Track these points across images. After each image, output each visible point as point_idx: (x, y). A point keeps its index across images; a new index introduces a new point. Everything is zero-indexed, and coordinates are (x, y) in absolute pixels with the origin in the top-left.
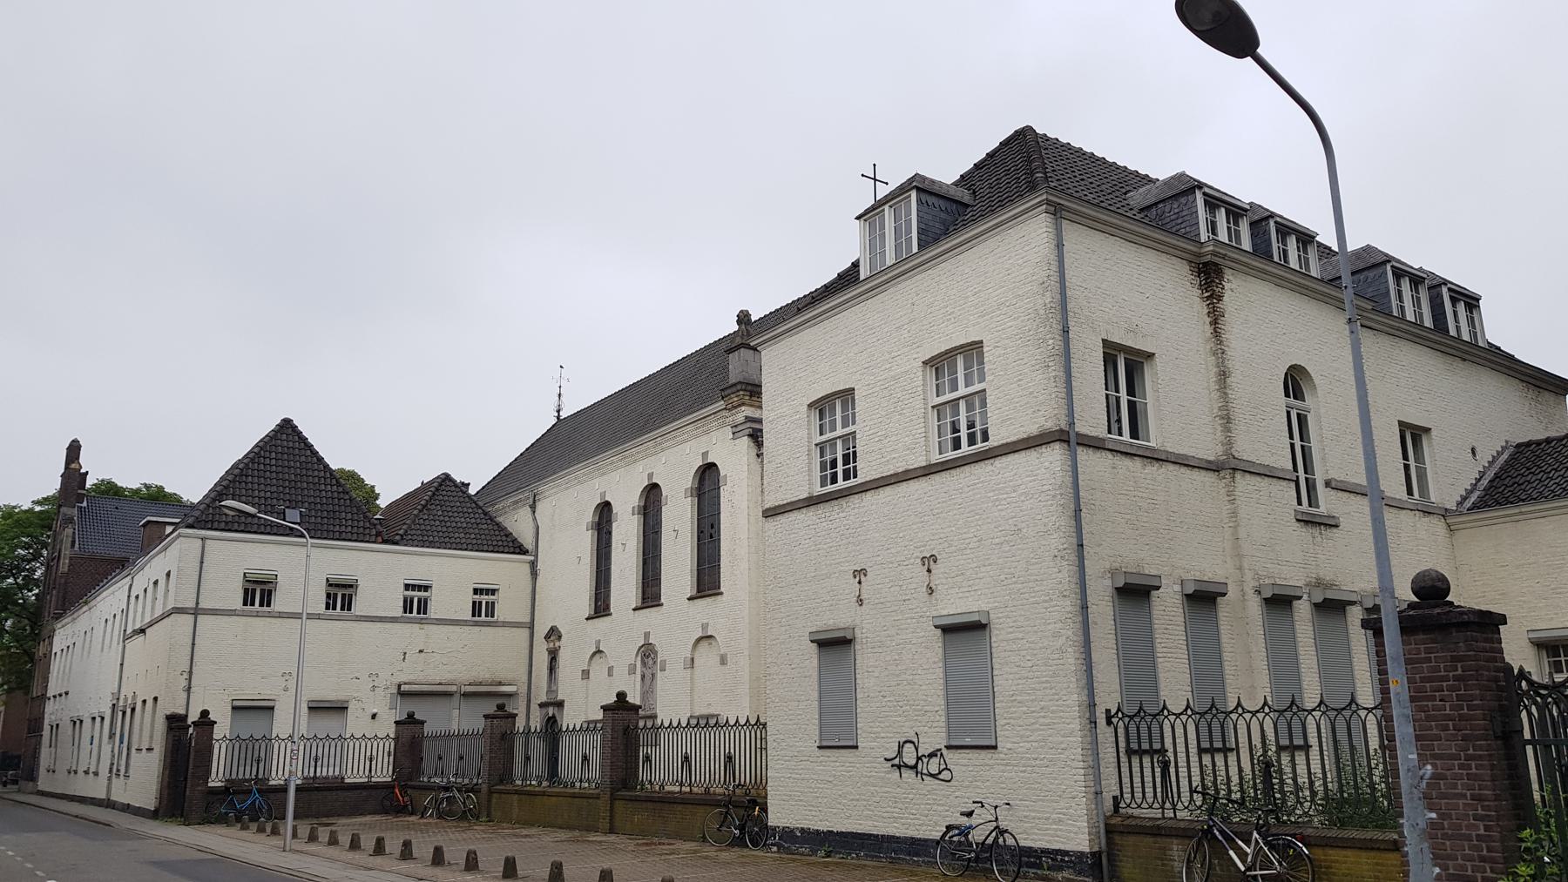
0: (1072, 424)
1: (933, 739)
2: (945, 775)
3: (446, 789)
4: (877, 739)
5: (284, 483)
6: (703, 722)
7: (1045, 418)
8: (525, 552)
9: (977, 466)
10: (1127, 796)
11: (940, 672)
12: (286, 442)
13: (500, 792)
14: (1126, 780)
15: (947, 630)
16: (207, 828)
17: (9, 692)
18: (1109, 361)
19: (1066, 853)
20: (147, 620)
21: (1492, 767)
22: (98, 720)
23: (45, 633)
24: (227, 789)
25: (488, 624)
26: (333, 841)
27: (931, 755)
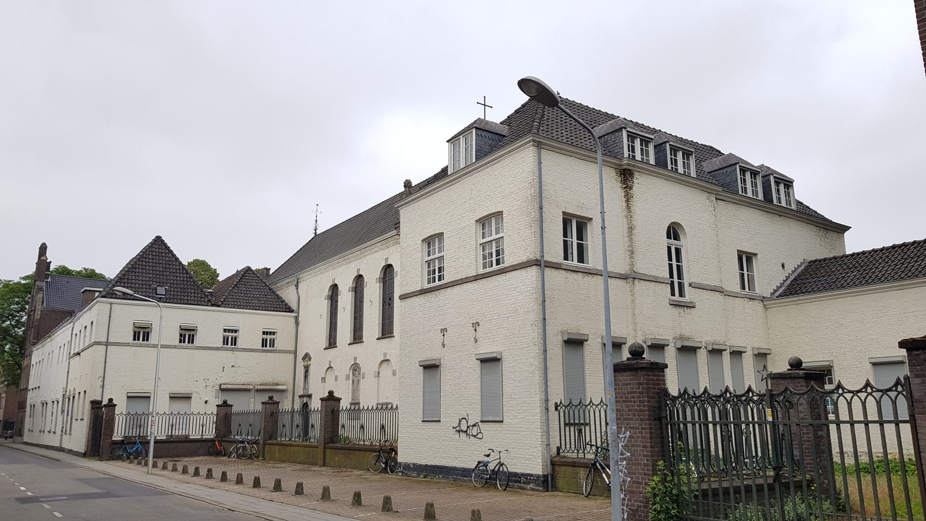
0: (542, 256)
1: (475, 418)
2: (480, 436)
3: (242, 442)
4: (449, 419)
6: (384, 407)
7: (530, 253)
8: (292, 311)
10: (563, 447)
11: (479, 383)
12: (158, 252)
13: (270, 444)
14: (563, 438)
15: (483, 361)
16: (111, 462)
17: (8, 386)
18: (566, 222)
19: (531, 475)
21: (651, 433)
23: (27, 353)
24: (123, 441)
25: (271, 351)
26: (175, 469)
27: (474, 426)
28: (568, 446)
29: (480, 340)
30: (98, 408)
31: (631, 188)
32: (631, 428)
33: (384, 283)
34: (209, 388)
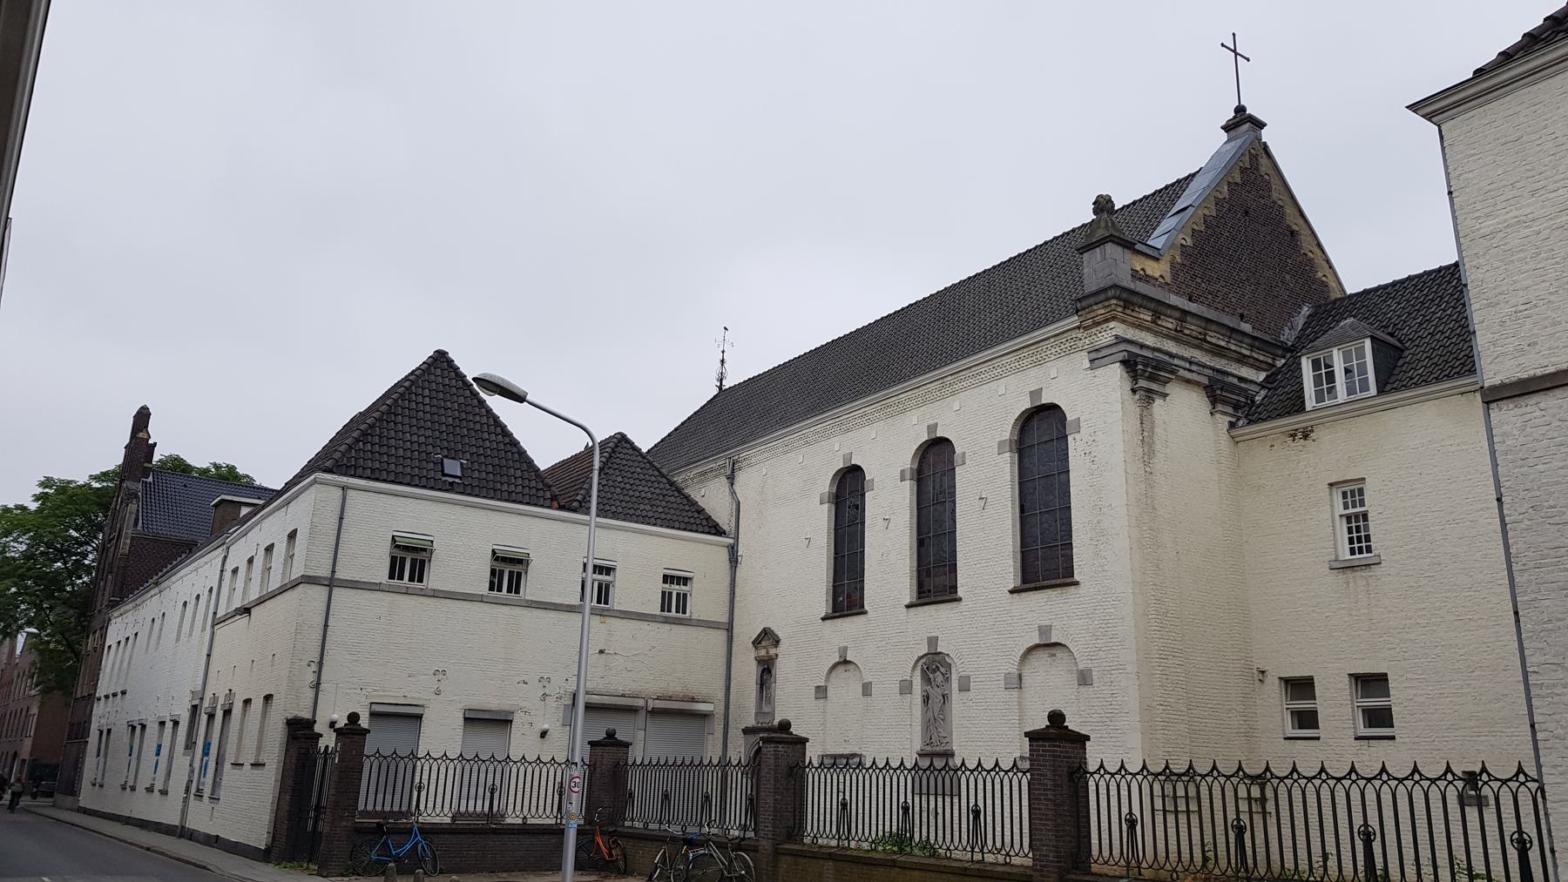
5: (432, 429)
20: (254, 595)
22: (169, 725)
23: (96, 624)
33: (1021, 452)
34: (551, 701)
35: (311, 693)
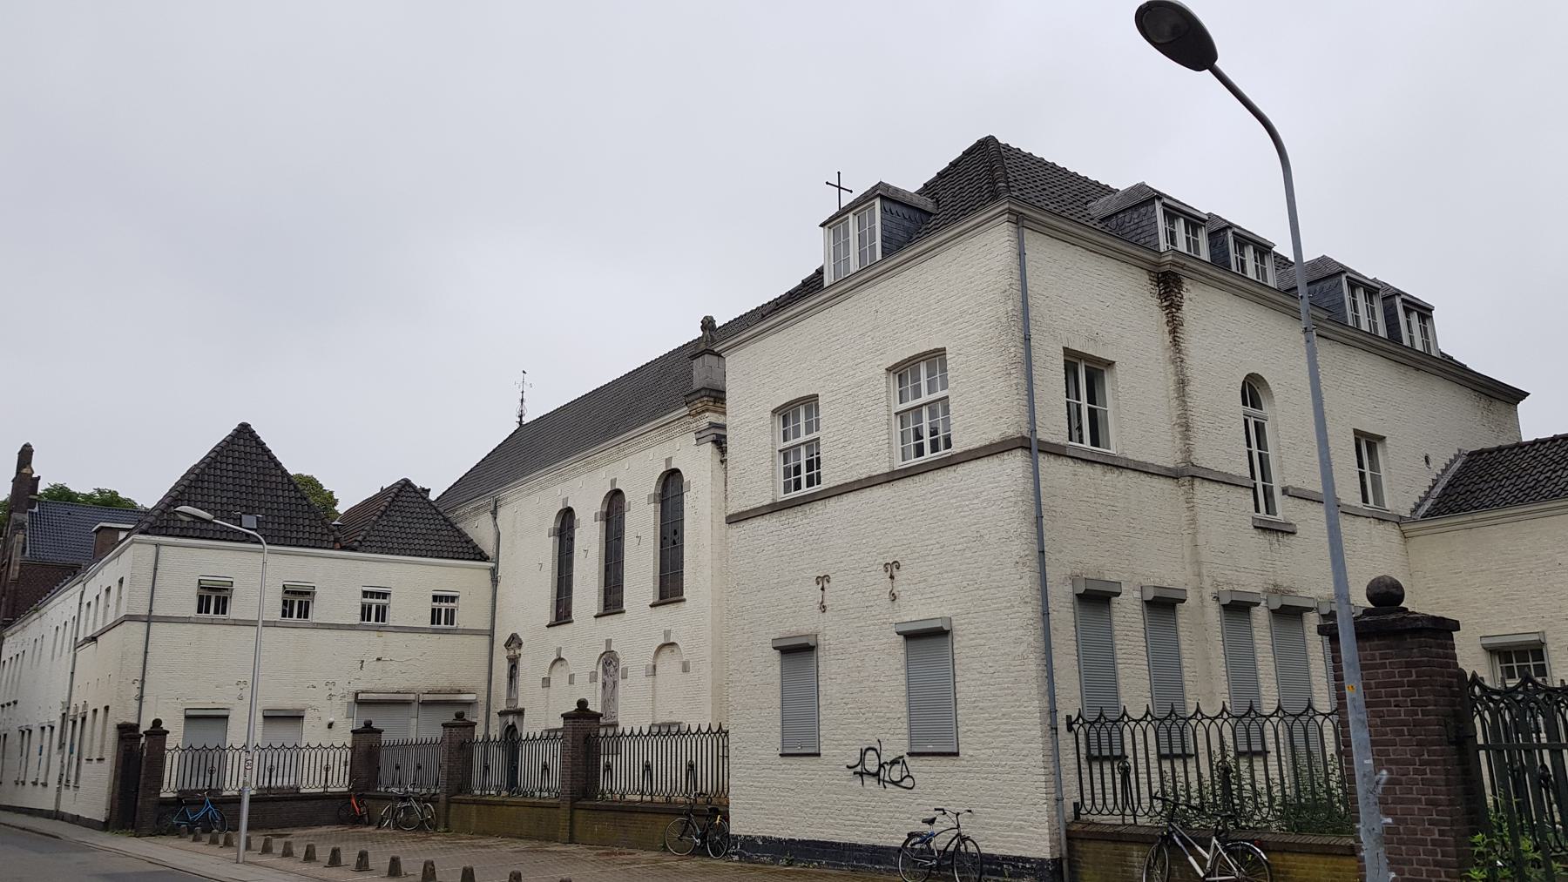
0: (1033, 431)
1: (896, 746)
2: (907, 782)
3: (404, 799)
4: (839, 747)
6: (664, 730)
7: (1007, 425)
8: (485, 559)
9: (940, 473)
10: (1088, 803)
11: (902, 679)
13: (460, 802)
14: (1087, 786)
15: (911, 636)
16: (158, 840)
18: (1070, 369)
19: (1027, 860)
20: (99, 627)
21: (1447, 772)
22: (48, 729)
24: (179, 800)
25: (447, 632)
27: (894, 762)
28: (1099, 801)
29: (903, 597)
30: (131, 738)
31: (1179, 308)
32: (1390, 762)
33: (607, 521)
35: (136, 704)
